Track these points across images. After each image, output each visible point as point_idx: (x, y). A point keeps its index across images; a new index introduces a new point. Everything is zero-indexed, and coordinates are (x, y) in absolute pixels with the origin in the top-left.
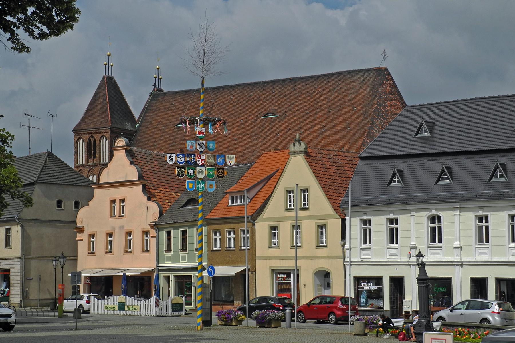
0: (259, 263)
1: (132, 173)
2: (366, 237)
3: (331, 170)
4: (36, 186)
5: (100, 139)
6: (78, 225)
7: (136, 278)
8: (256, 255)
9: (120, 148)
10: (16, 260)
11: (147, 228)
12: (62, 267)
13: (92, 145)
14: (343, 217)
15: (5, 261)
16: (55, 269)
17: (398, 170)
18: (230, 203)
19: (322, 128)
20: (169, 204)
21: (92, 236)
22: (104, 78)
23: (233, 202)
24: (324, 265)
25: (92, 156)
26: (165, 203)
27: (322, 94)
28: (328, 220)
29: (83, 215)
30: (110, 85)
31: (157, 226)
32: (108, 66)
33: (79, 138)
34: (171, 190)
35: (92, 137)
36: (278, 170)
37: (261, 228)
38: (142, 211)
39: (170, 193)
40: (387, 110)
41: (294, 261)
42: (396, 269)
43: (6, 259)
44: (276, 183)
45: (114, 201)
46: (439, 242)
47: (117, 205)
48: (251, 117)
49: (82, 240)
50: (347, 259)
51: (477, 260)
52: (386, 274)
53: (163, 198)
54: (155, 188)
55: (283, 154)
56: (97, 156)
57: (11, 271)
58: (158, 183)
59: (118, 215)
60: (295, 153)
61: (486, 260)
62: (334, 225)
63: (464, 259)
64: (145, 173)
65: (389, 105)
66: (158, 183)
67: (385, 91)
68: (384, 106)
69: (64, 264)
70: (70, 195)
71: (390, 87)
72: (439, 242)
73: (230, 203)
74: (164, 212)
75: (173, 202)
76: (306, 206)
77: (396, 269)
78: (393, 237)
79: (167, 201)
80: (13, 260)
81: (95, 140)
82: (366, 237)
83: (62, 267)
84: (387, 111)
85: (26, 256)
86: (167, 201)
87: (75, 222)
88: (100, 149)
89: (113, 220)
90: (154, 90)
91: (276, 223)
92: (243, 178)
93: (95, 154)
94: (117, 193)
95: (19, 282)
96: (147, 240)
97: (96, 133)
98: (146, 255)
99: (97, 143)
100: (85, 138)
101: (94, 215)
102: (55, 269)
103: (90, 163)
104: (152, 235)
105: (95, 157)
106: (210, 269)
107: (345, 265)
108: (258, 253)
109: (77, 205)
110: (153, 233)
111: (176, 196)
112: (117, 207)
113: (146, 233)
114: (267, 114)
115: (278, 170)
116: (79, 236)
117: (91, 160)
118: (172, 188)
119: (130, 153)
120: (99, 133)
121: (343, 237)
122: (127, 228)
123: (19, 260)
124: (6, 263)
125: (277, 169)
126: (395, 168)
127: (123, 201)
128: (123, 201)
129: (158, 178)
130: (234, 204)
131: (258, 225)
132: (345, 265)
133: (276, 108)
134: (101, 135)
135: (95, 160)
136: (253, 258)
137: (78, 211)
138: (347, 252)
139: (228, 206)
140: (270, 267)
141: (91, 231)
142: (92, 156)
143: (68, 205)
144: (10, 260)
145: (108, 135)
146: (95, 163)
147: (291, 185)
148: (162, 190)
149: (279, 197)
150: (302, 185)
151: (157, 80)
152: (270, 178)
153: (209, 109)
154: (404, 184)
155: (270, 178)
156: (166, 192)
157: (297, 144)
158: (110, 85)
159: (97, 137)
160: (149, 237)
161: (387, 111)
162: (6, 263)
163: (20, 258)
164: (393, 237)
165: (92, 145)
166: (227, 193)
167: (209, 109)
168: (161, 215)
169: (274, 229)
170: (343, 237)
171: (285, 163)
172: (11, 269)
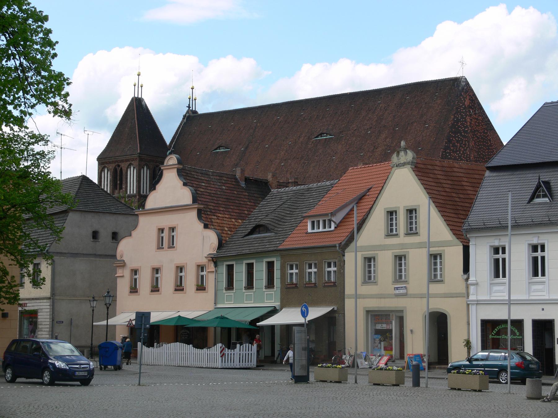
0: (349, 304)
1: (185, 196)
2: (499, 269)
3: (445, 185)
4: (71, 215)
5: (127, 168)
6: (118, 259)
7: (547, 336)
8: (346, 293)
9: (171, 167)
10: (45, 301)
11: (204, 261)
12: (108, 308)
13: (118, 174)
14: (465, 244)
15: (33, 301)
16: (93, 310)
17: (543, 182)
18: (310, 230)
19: (386, 149)
20: (229, 232)
21: (135, 272)
22: (132, 99)
23: (313, 228)
24: (438, 305)
25: (118, 186)
26: (224, 232)
27: (386, 110)
28: (445, 248)
29: (125, 248)
30: (138, 108)
31: (215, 260)
32: (138, 86)
33: (104, 167)
34: (230, 217)
35: (119, 166)
36: (371, 188)
37: (352, 261)
38: (197, 241)
39: (229, 220)
40: (467, 126)
41: (354, 300)
42: (543, 309)
43: (33, 299)
44: (372, 203)
45: (162, 230)
46: (503, 277)
47: (165, 235)
48: (301, 139)
49: (123, 276)
50: (472, 297)
51: (492, 298)
52: (528, 316)
53: (221, 225)
54: (212, 214)
55: (377, 168)
56: (124, 187)
57: (39, 314)
58: (216, 208)
59: (167, 247)
60: (399, 166)
61: (501, 298)
62: (453, 255)
63: (480, 298)
64: (200, 196)
65: (469, 120)
66: (216, 208)
67: (464, 104)
68: (463, 121)
69: (110, 304)
70: (106, 224)
71: (469, 99)
72: (503, 277)
73: (310, 230)
74: (224, 242)
75: (232, 229)
76: (394, 232)
77: (543, 309)
78: (538, 267)
79: (226, 229)
80: (41, 301)
81: (121, 168)
82: (499, 269)
83: (108, 308)
84: (467, 127)
85: (53, 298)
86: (226, 229)
87: (114, 256)
88: (127, 178)
89: (161, 252)
90: (188, 112)
91: (373, 252)
92: (324, 199)
93: (121, 184)
94: (166, 221)
95: (48, 326)
96: (202, 276)
97: (122, 161)
98: (201, 294)
99: (124, 172)
100: (111, 167)
101: (138, 248)
102: (93, 310)
103: (116, 195)
104: (209, 270)
105: (121, 188)
106: (303, 309)
107: (468, 305)
108: (349, 289)
109: (115, 237)
110: (212, 267)
111: (236, 223)
112: (166, 239)
113: (201, 268)
114: (321, 135)
115: (371, 188)
116: (119, 272)
117: (117, 191)
118: (232, 214)
119: (181, 173)
120: (127, 160)
121: (466, 269)
122: (180, 262)
123: (48, 301)
124: (33, 304)
125: (370, 187)
126: (539, 179)
127: (173, 229)
128: (173, 229)
129: (215, 202)
130: (315, 231)
131: (349, 257)
132: (468, 305)
133: (330, 127)
134: (129, 163)
135: (121, 191)
136: (341, 298)
137: (118, 243)
138: (472, 288)
139: (307, 233)
140: (364, 308)
141: (134, 266)
142: (118, 186)
143: (106, 236)
144: (38, 301)
145: (136, 163)
146: (121, 194)
147: (391, 206)
148: (220, 215)
149: (377, 221)
150: (411, 204)
151: (191, 101)
152: (360, 199)
153: (251, 131)
154: (552, 199)
155: (360, 199)
156: (225, 219)
157: (402, 153)
158: (138, 108)
159: (124, 165)
160: (204, 273)
161: (467, 127)
162: (33, 304)
163: (49, 298)
164: (538, 267)
165: (118, 174)
166: (305, 217)
167: (251, 131)
168: (221, 245)
169: (369, 260)
170: (466, 269)
171: (386, 178)
172: (39, 311)
